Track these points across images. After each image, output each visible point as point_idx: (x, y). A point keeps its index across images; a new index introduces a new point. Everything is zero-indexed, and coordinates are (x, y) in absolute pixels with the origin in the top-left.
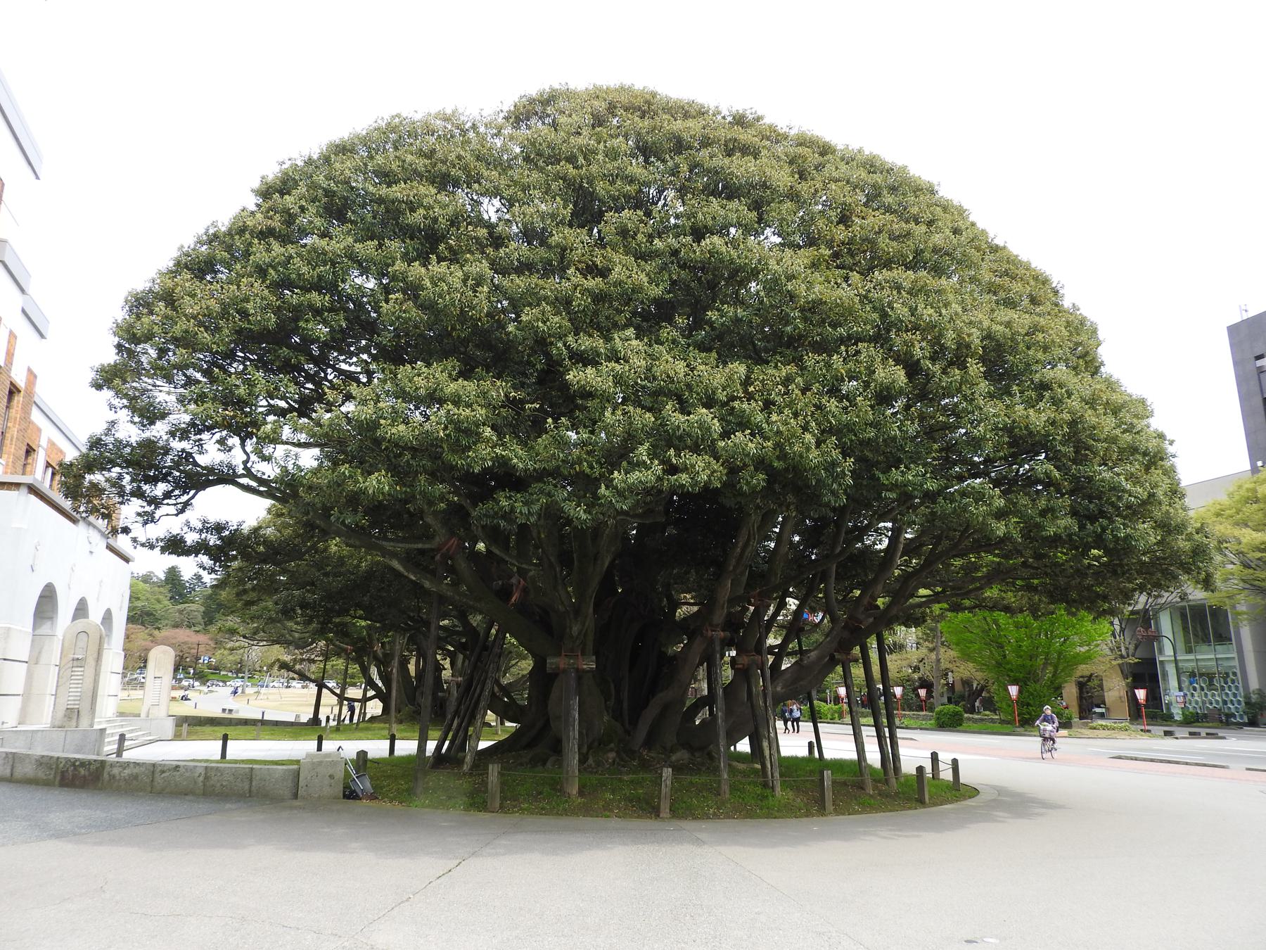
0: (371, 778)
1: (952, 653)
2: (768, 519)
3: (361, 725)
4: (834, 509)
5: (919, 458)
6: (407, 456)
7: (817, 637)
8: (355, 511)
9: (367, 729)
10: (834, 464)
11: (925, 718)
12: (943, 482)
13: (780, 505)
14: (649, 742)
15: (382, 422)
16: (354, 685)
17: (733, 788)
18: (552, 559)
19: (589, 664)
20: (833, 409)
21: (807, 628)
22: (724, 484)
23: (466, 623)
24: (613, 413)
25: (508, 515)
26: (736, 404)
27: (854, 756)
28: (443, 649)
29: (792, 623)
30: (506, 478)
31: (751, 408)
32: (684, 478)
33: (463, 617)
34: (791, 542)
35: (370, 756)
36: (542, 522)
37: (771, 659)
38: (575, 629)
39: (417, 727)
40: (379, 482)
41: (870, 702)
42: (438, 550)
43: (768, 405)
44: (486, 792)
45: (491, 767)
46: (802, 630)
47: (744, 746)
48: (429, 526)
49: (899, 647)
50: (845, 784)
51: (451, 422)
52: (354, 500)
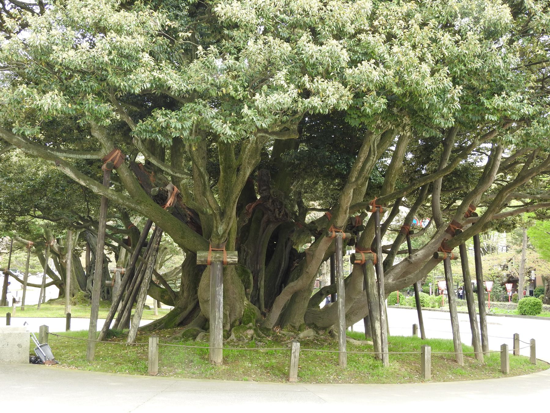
0: (52, 348)
1: (537, 255)
2: (386, 136)
3: (42, 306)
4: (443, 131)
5: (519, 87)
6: (77, 77)
7: (424, 239)
8: (33, 125)
9: (47, 309)
10: (444, 91)
11: (509, 307)
12: (538, 108)
13: (397, 126)
14: (281, 323)
15: (54, 47)
16: (34, 273)
17: (350, 360)
18: (202, 170)
19: (232, 257)
20: (447, 42)
21: (416, 231)
22: (351, 107)
23: (128, 223)
24: (255, 42)
25: (164, 130)
26: (362, 36)
27: (451, 337)
28: (109, 245)
29: (403, 228)
30: (163, 99)
31: (376, 42)
32: (315, 101)
33: (125, 217)
34: (405, 160)
35: (50, 331)
36: (193, 137)
37: (384, 256)
38: (221, 229)
39: (89, 308)
40: (53, 99)
41: (466, 295)
42: (104, 160)
43: (390, 37)
44: (147, 359)
45: (150, 339)
46: (411, 233)
47: (359, 327)
48: (97, 141)
49: (491, 249)
50: (442, 358)
51: (115, 48)
52: (31, 116)
